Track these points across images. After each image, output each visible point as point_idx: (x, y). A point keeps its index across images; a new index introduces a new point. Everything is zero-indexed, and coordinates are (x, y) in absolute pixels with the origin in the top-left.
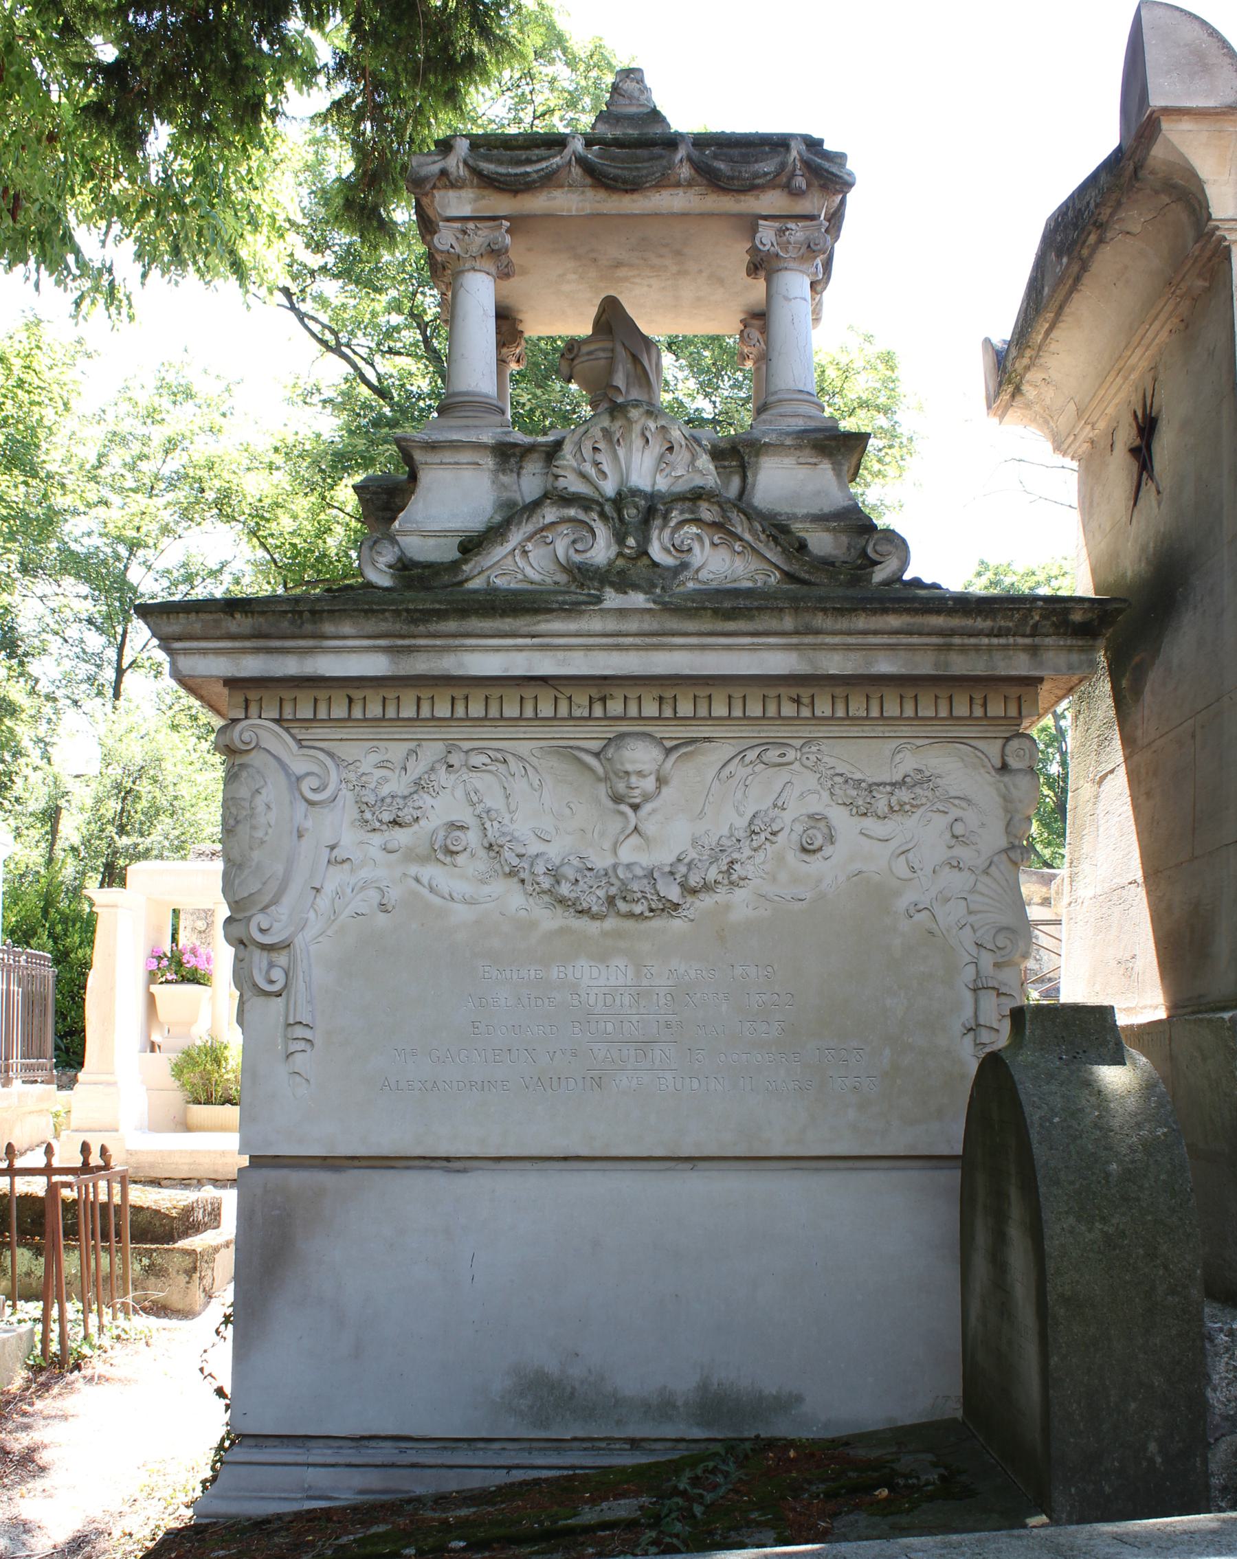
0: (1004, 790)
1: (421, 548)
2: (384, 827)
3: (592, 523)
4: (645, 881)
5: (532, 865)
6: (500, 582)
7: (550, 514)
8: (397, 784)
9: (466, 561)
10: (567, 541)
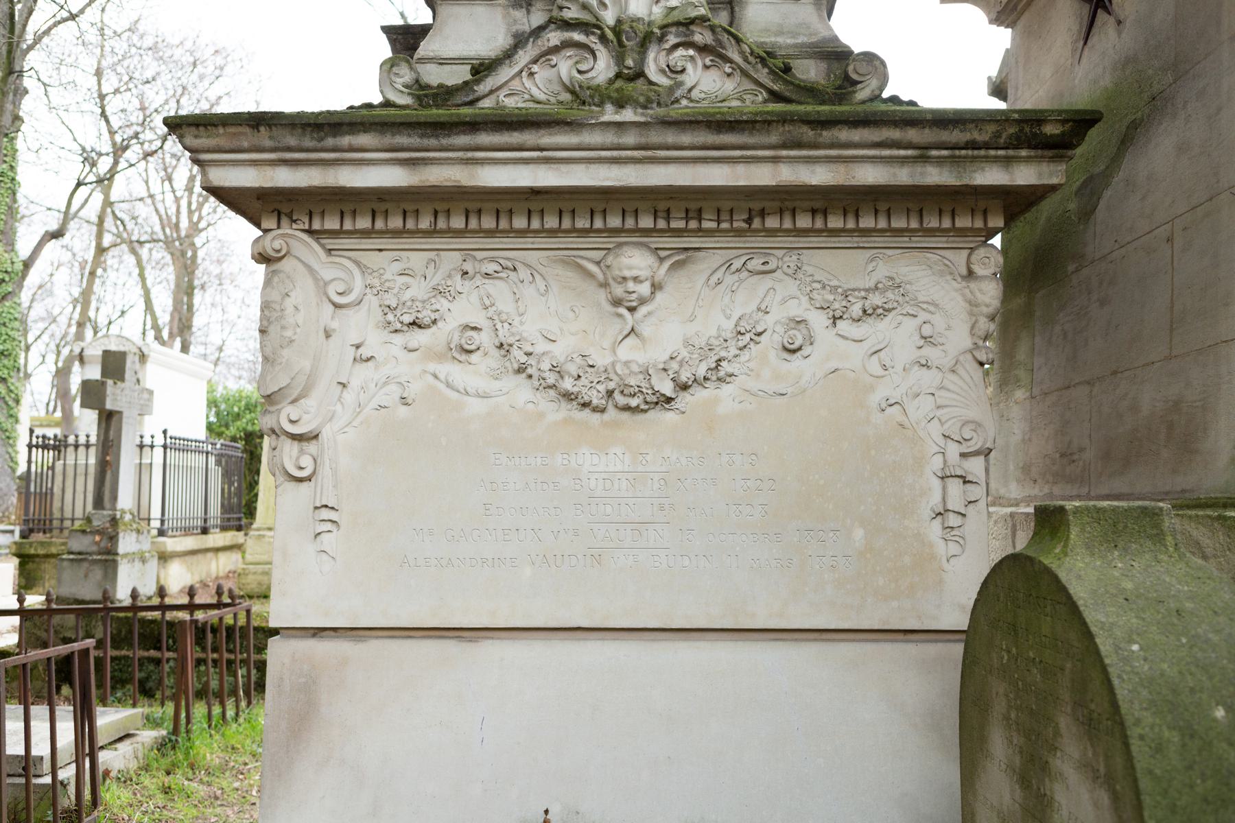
0: (969, 295)
1: (435, 76)
2: (405, 328)
3: (593, 46)
4: (641, 377)
5: (538, 362)
6: (511, 103)
7: (554, 37)
8: (418, 290)
9: (478, 82)
10: (570, 62)
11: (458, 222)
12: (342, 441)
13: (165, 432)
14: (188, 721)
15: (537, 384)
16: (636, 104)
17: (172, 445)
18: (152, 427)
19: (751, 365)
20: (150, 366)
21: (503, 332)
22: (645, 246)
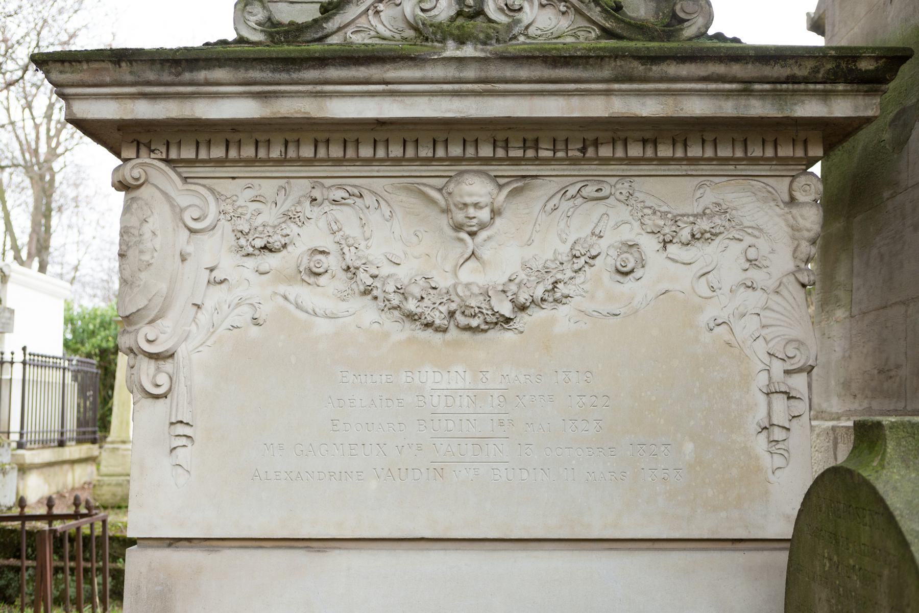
2: (257, 252)
4: (482, 298)
5: (384, 284)
9: (327, 19)
11: (307, 152)
12: (197, 359)
13: (24, 349)
15: (382, 305)
16: (476, 40)
17: (31, 361)
22: (485, 174)
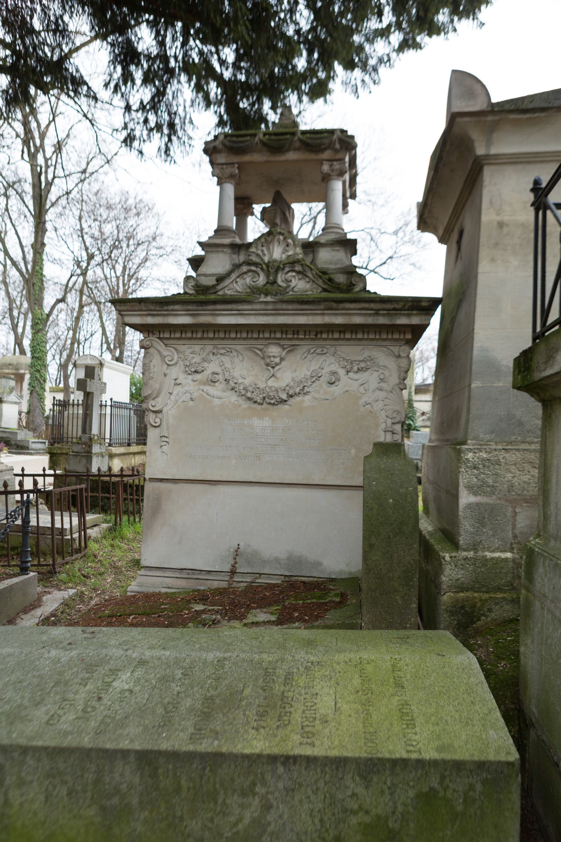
7: (245, 268)
8: (197, 359)
9: (217, 285)
11: (211, 335)
12: (170, 412)
13: (111, 399)
14: (120, 520)
16: (272, 295)
17: (116, 405)
18: (106, 398)
19: (316, 388)
20: (105, 370)
21: (227, 374)
22: (279, 344)
